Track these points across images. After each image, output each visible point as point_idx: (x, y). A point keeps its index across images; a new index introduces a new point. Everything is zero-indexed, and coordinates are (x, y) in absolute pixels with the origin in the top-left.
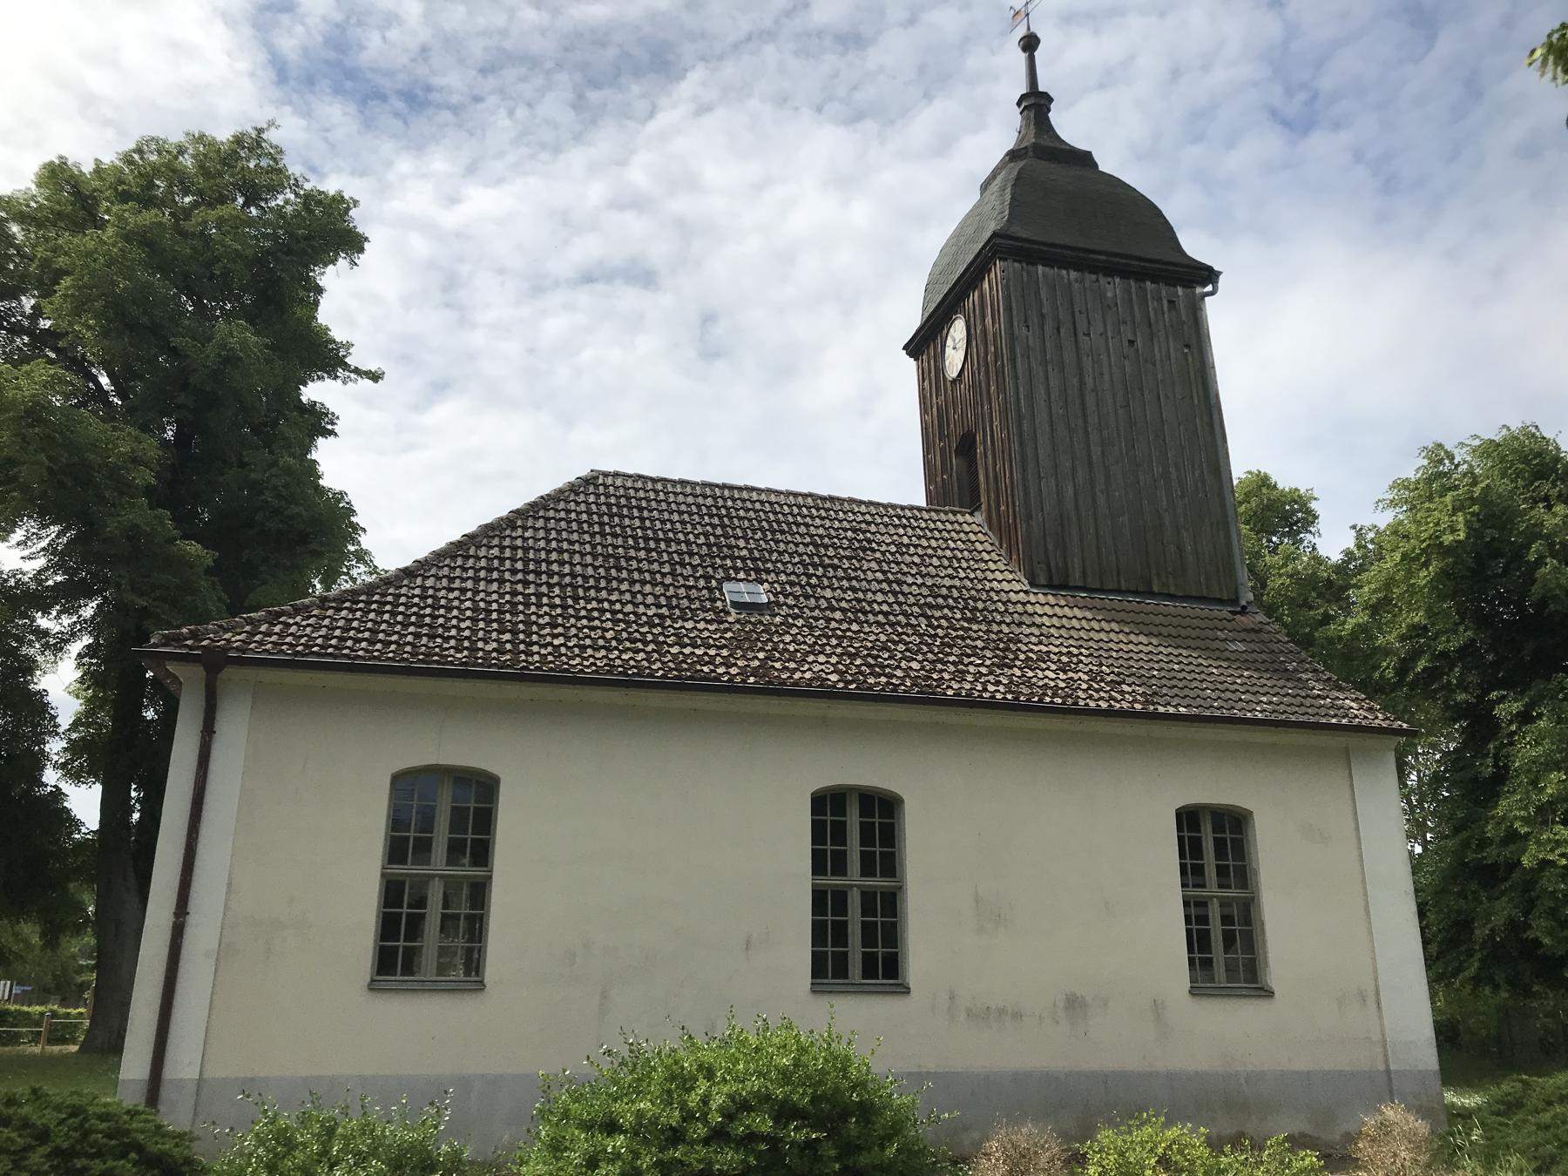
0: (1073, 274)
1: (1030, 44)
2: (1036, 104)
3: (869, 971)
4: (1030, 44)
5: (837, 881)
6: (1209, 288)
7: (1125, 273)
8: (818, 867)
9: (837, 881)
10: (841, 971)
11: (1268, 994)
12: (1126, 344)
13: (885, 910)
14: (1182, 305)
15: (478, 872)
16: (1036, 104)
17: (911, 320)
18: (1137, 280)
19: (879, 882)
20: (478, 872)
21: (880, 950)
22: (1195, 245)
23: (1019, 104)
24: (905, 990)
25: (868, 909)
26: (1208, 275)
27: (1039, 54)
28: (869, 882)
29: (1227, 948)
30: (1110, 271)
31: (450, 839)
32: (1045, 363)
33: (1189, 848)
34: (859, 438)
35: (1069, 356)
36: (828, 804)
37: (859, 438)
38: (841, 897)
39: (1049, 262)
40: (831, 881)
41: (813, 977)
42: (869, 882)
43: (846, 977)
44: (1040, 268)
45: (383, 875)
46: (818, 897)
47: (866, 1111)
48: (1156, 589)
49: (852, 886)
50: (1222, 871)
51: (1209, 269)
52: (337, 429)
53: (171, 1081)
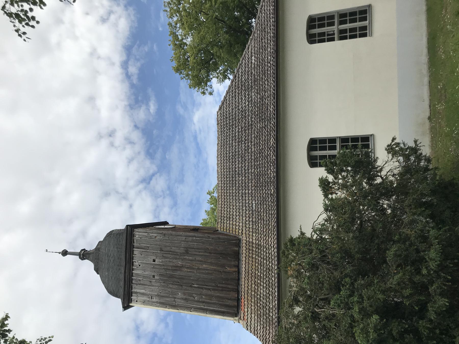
2: (84, 255)
3: (365, 19)
4: (65, 253)
10: (365, 28)
13: (345, 16)
15: (338, 141)
24: (370, 6)
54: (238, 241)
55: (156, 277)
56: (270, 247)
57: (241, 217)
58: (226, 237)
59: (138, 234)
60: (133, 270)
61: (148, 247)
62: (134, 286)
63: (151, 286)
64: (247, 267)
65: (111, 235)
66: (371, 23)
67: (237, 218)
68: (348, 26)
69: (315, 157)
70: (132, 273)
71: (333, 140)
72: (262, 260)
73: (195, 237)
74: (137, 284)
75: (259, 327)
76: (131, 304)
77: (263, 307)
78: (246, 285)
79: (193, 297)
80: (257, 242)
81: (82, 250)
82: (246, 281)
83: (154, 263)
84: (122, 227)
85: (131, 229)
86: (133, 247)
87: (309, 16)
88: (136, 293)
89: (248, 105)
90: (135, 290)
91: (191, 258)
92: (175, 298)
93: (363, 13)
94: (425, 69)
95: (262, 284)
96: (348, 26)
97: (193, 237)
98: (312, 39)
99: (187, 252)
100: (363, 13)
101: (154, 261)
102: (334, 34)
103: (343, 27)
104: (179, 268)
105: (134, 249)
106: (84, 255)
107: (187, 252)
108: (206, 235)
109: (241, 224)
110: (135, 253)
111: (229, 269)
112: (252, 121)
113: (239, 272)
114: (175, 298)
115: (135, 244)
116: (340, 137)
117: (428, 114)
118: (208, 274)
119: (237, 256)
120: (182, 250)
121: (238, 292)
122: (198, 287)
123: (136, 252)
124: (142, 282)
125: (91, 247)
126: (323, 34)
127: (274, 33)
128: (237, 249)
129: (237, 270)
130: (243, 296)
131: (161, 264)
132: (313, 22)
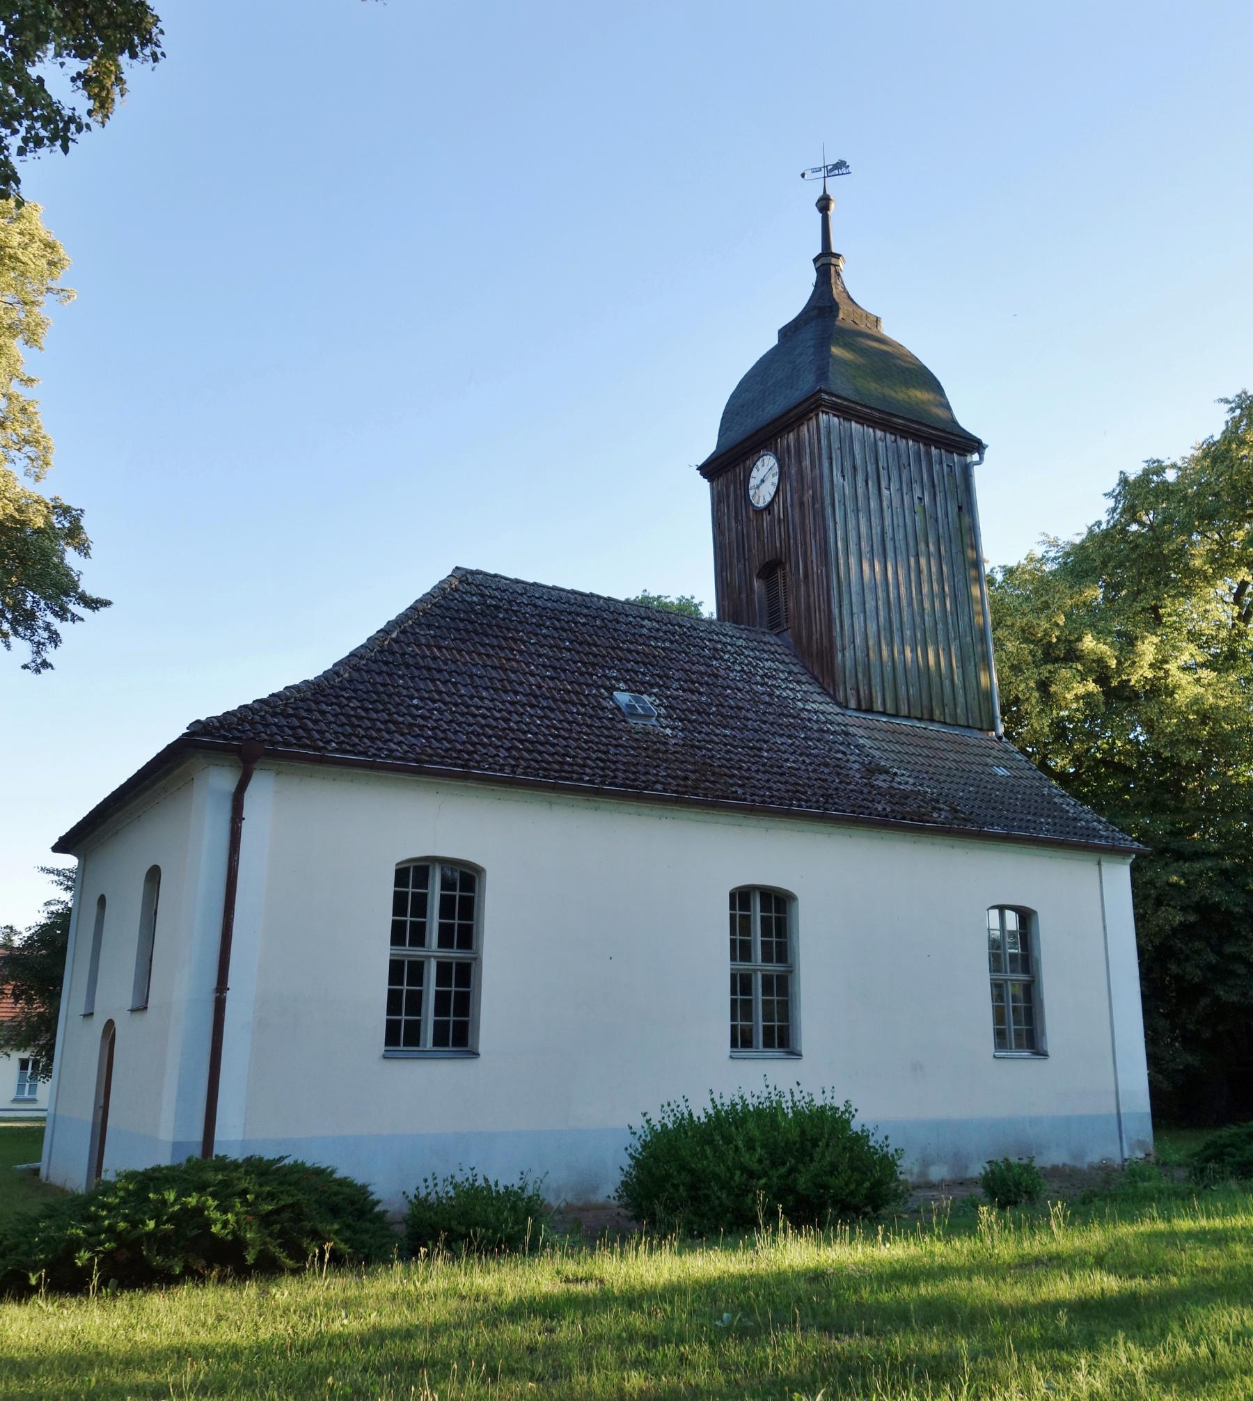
0: (879, 434)
2: (826, 263)
3: (440, 1039)
6: (976, 457)
7: (917, 437)
10: (413, 1038)
11: (1043, 1054)
12: (916, 501)
14: (957, 470)
16: (826, 263)
17: (707, 445)
18: (925, 444)
21: (403, 1017)
22: (968, 418)
23: (815, 260)
24: (475, 1054)
25: (767, 989)
26: (977, 446)
29: (438, 1012)
30: (905, 433)
32: (857, 511)
33: (740, 925)
34: (664, 555)
35: (873, 504)
36: (411, 876)
37: (664, 555)
38: (417, 971)
39: (863, 420)
41: (387, 1044)
43: (417, 1044)
44: (854, 424)
47: (324, 1171)
48: (948, 720)
49: (429, 957)
51: (979, 442)
53: (173, 1156)
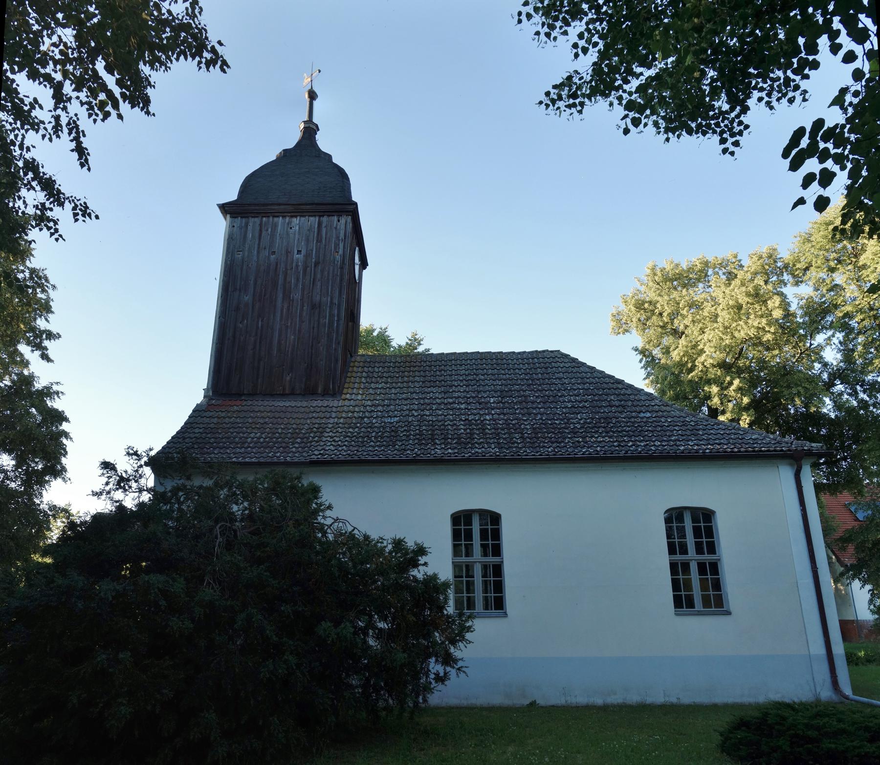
1: (312, 96)
2: (310, 130)
3: (706, 602)
4: (312, 96)
5: (683, 557)
8: (672, 550)
9: (683, 557)
10: (691, 604)
13: (711, 571)
15: (496, 559)
19: (706, 557)
20: (496, 559)
24: (505, 615)
27: (315, 103)
28: (701, 557)
31: (481, 530)
36: (674, 517)
40: (678, 557)
42: (701, 557)
45: (453, 563)
46: (673, 566)
50: (484, 547)
52: (604, 113)
54: (331, 392)
55: (273, 257)
56: (320, 448)
57: (372, 397)
58: (339, 372)
59: (345, 221)
60: (284, 217)
61: (321, 241)
62: (257, 220)
63: (259, 248)
64: (303, 410)
65: (342, 176)
66: (700, 613)
67: (371, 391)
68: (478, 580)
69: (469, 522)
70: (278, 217)
71: (497, 551)
72: (301, 435)
73: (338, 321)
74: (261, 225)
75: (197, 431)
76: (228, 216)
77: (229, 438)
78: (262, 408)
79: (243, 320)
80: (330, 426)
81: (317, 126)
82: (268, 409)
83: (296, 252)
84: (356, 196)
85: (351, 210)
86: (320, 216)
87: (452, 515)
88: (247, 225)
89: (566, 407)
90: (251, 224)
91: (304, 314)
92: (240, 290)
93: (715, 601)
94: (634, 698)
95: (263, 436)
96: (478, 580)
97: (338, 315)
98: (674, 517)
99: (313, 306)
100: (715, 601)
101: (299, 252)
102: (467, 555)
103: (694, 567)
104: (287, 295)
105: (317, 218)
106: (310, 130)
107: (313, 306)
108: (342, 339)
109: (359, 397)
110: (312, 219)
111: (288, 378)
112: (536, 414)
113: (283, 395)
114: (240, 290)
115: (325, 219)
116: (502, 562)
117: (541, 702)
118: (279, 342)
119: (310, 392)
120: (317, 298)
121: (253, 394)
122: (258, 327)
123: (314, 220)
124: (264, 233)
125: (323, 142)
126: (469, 536)
127: (697, 451)
128: (320, 391)
129: (287, 392)
130: (245, 403)
131: (294, 264)
132: (704, 518)
